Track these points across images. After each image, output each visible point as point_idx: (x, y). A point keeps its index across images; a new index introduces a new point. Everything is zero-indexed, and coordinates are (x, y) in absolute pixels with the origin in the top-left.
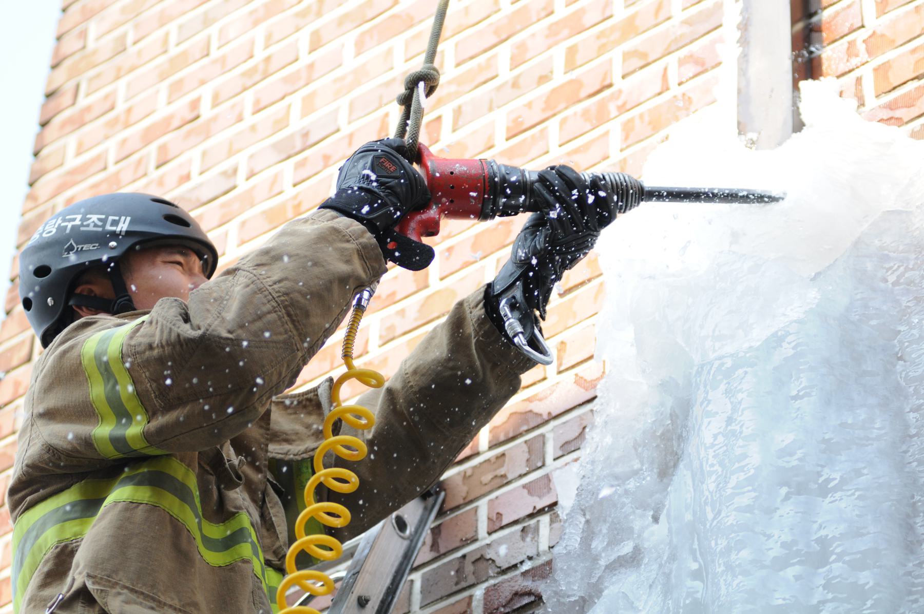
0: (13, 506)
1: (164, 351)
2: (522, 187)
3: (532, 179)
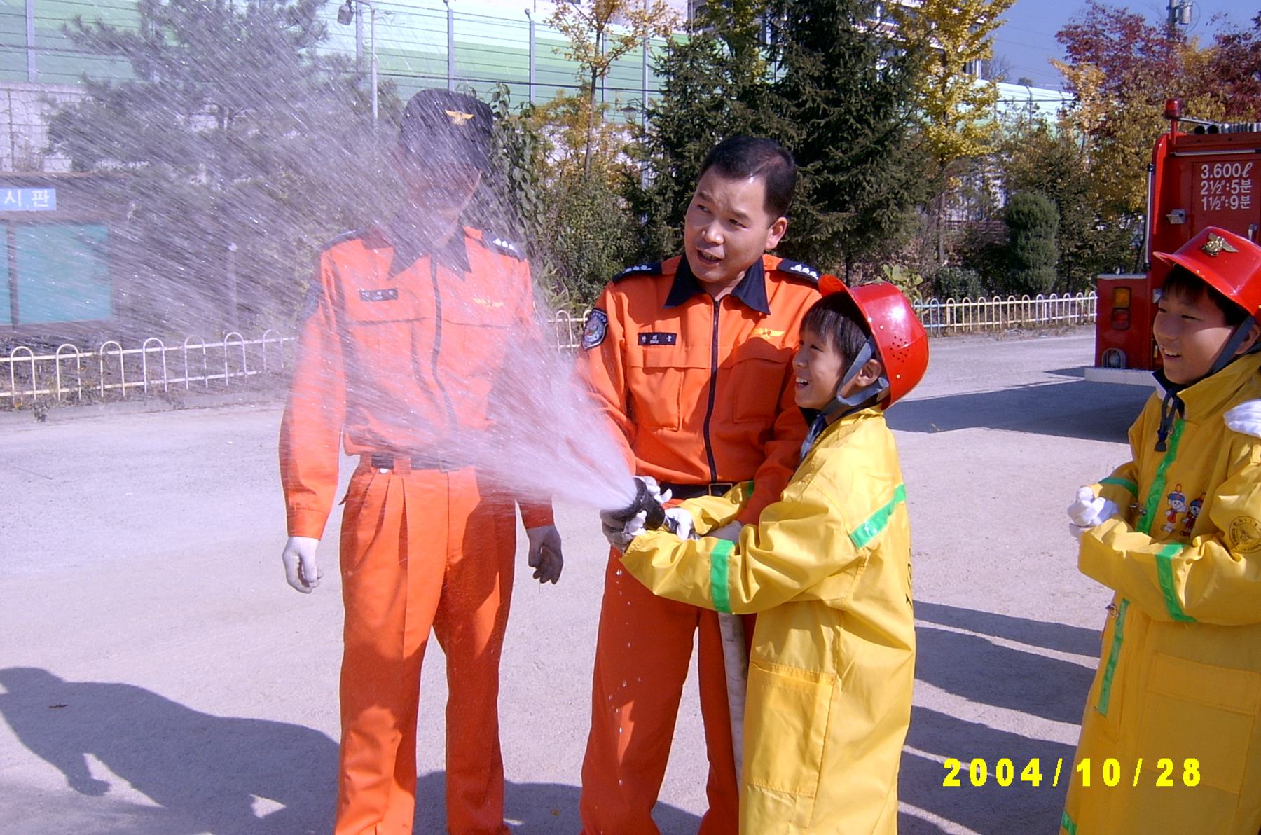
0: (633, 392)
1: (221, 126)
2: (804, 729)
3: (536, 32)
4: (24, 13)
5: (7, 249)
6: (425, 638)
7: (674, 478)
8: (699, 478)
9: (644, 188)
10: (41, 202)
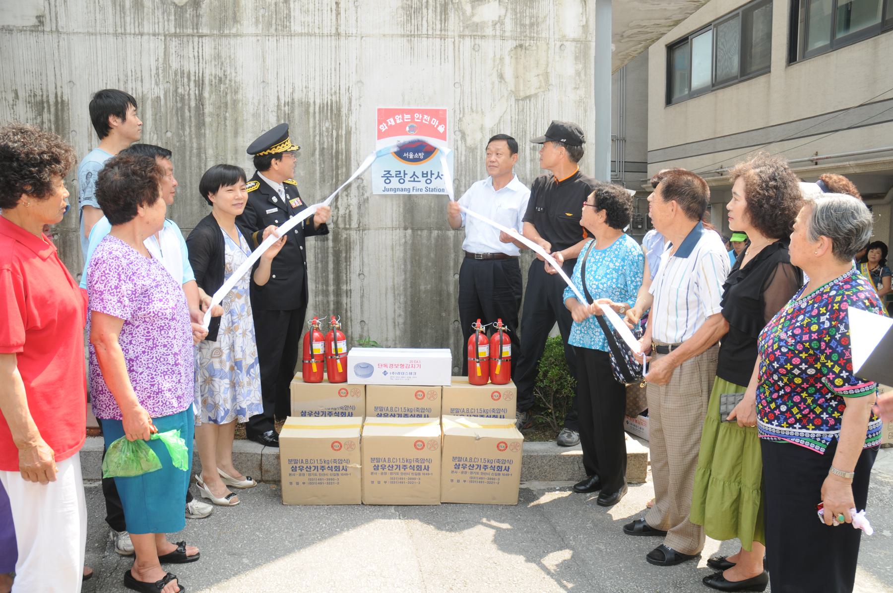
4: (275, 477)
5: (273, 2)
6: (491, 143)
7: (108, 348)
9: (56, 249)
10: (426, 120)
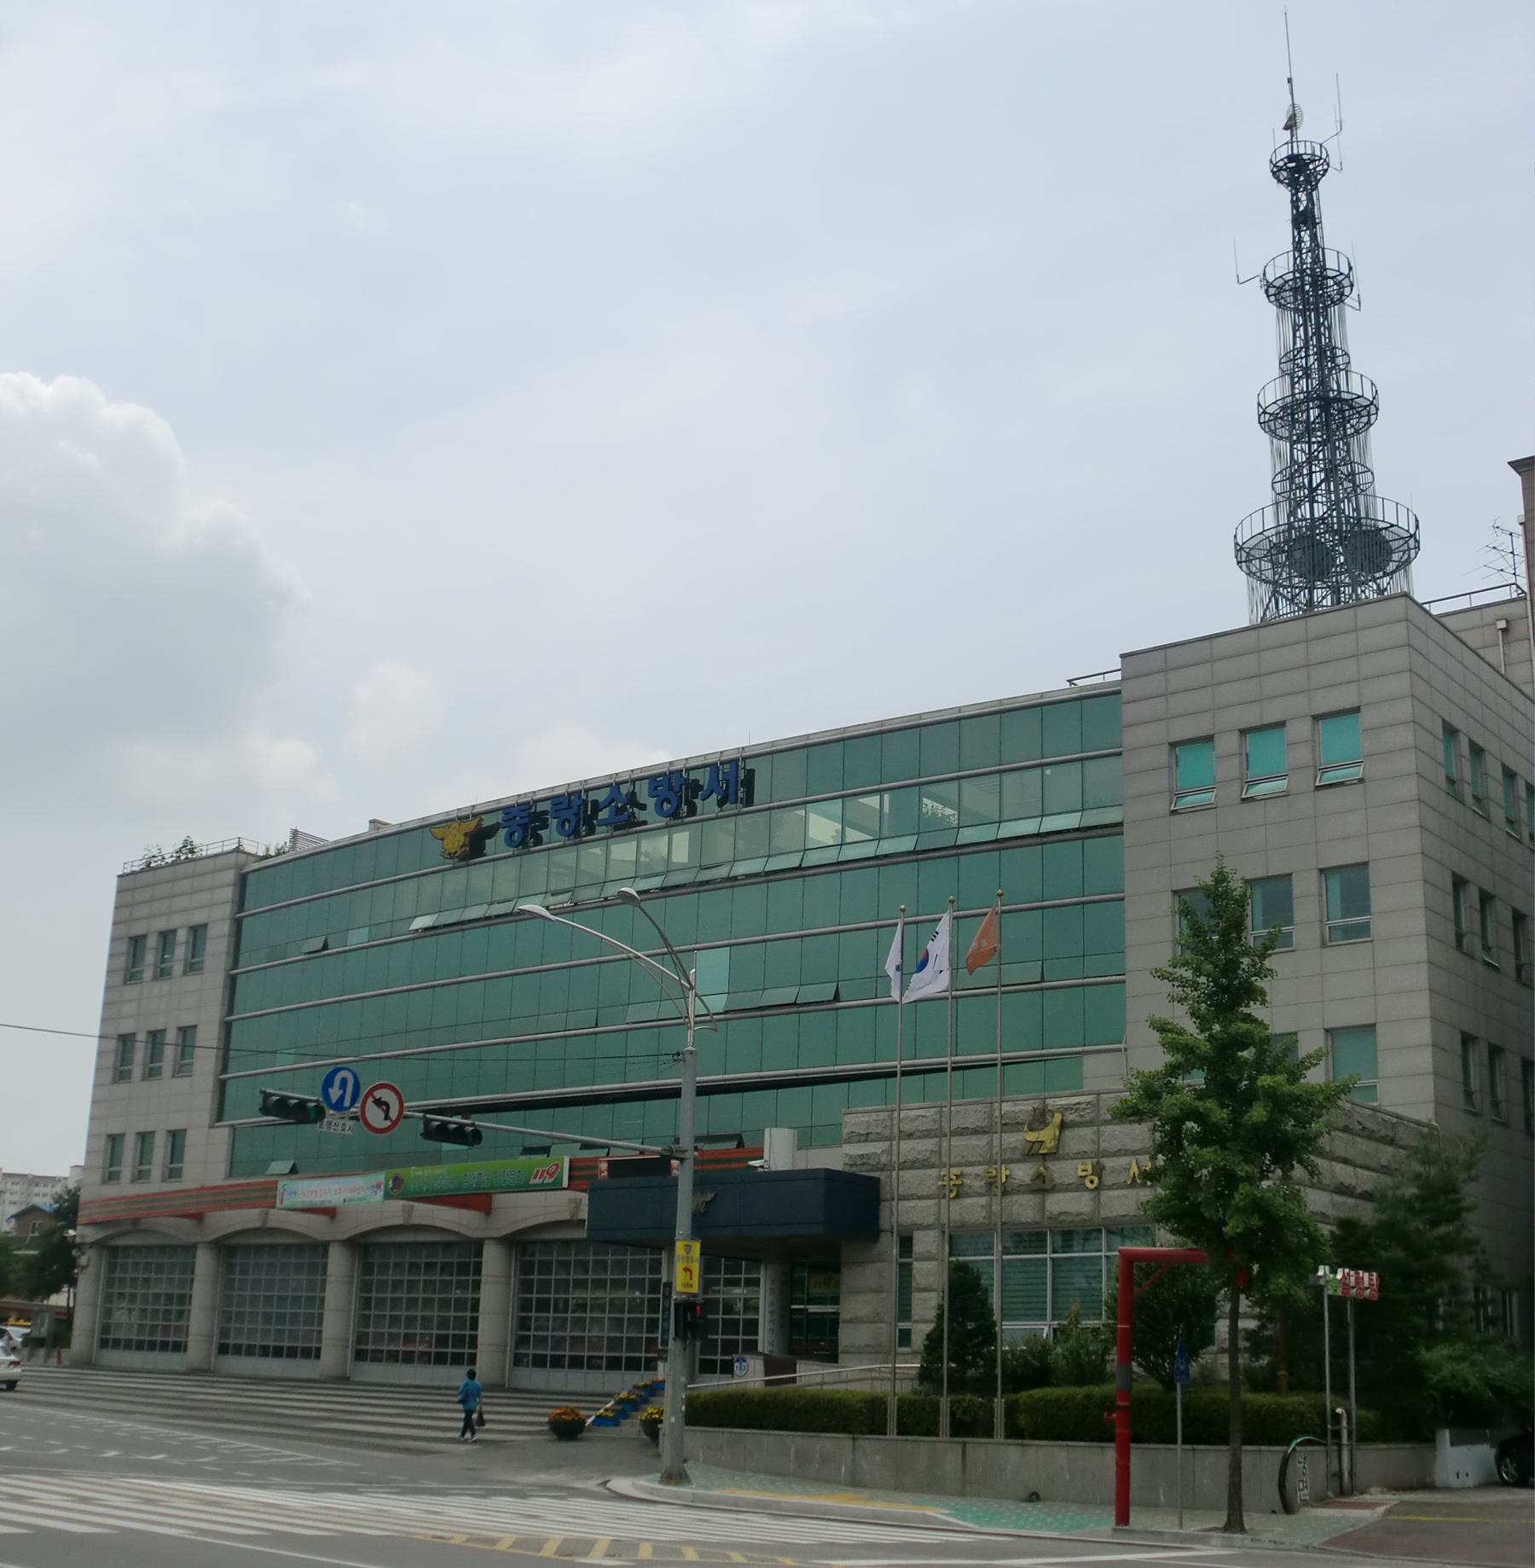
4: (1046, 812)
8: (637, 1482)
